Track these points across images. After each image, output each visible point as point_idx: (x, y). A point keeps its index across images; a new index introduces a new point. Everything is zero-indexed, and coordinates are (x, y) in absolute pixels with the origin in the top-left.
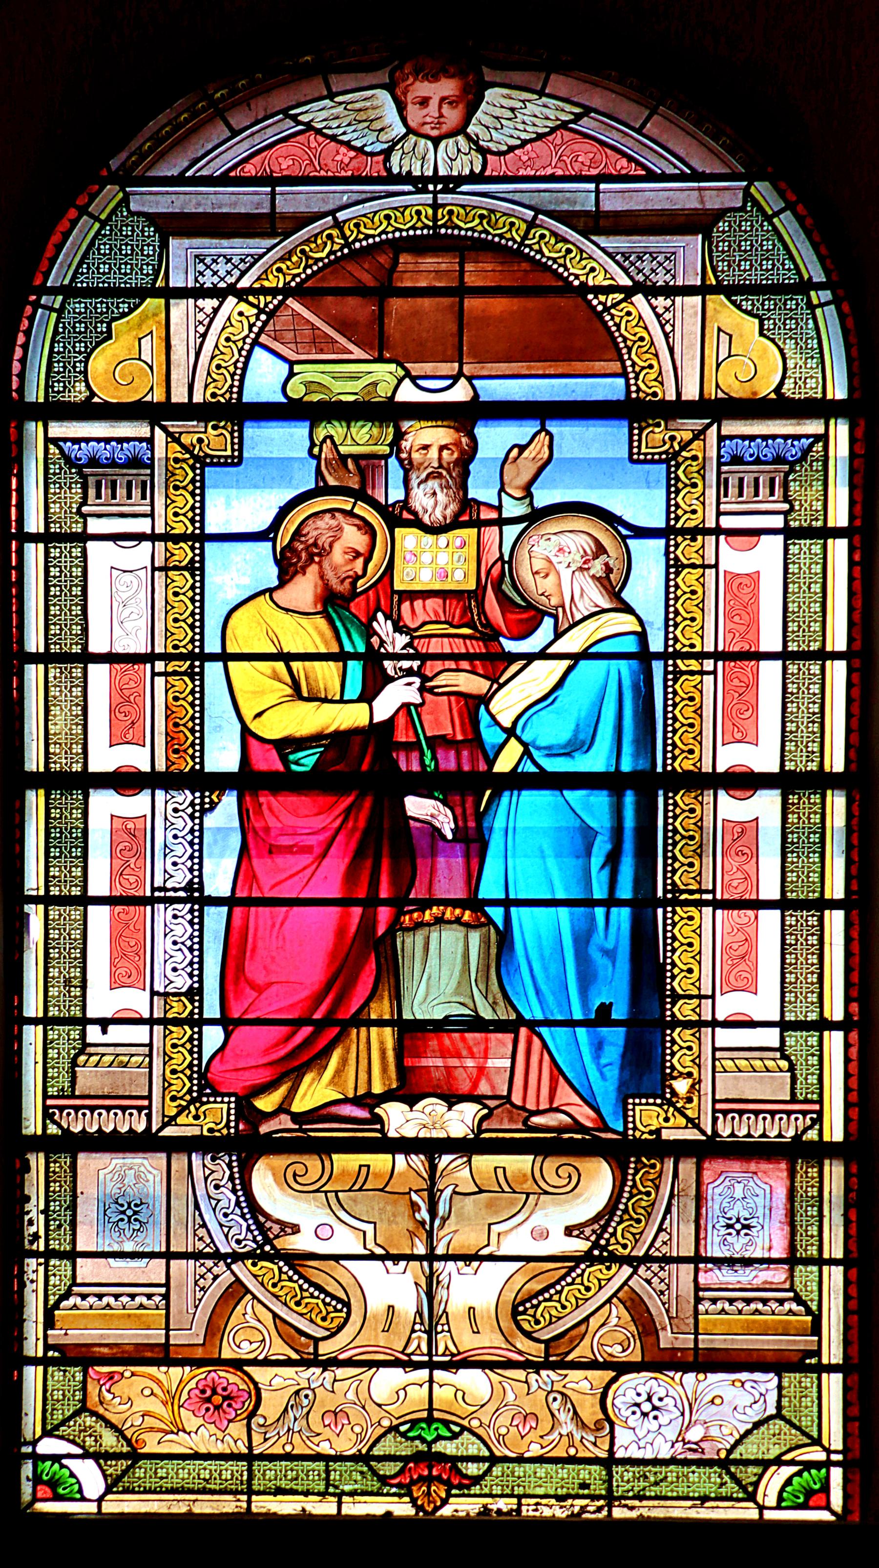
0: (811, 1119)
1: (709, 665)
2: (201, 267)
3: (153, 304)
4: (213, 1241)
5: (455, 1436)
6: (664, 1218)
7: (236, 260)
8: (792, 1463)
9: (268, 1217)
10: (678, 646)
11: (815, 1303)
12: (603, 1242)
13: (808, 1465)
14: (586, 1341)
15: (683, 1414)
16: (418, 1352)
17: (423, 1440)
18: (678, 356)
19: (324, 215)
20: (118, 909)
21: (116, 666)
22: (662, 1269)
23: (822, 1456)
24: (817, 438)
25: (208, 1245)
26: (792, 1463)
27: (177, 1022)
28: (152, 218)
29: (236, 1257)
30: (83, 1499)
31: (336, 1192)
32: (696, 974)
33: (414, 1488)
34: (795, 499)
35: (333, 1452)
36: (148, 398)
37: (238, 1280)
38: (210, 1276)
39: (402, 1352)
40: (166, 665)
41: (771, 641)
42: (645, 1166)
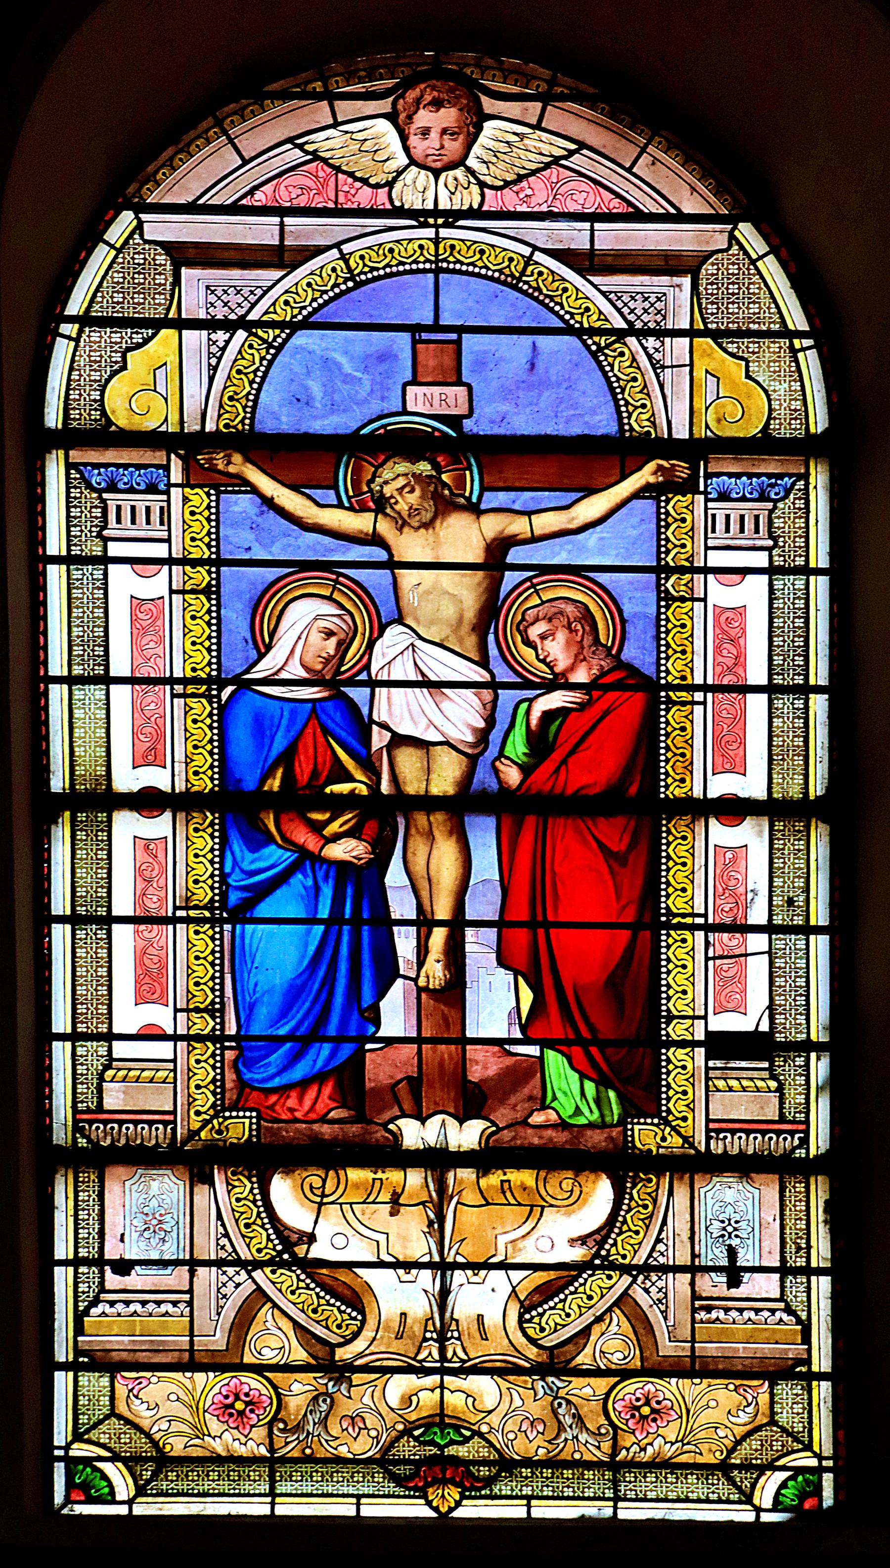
0: (799, 1138)
1: (699, 696)
2: (212, 298)
3: (168, 335)
4: (235, 1251)
5: (467, 1440)
6: (661, 1231)
7: (245, 292)
8: (784, 1468)
9: (287, 1228)
10: (670, 678)
11: (805, 1313)
12: (603, 1253)
13: (799, 1471)
14: (588, 1350)
15: (681, 1417)
16: (430, 1359)
17: (435, 1444)
18: (668, 392)
19: (328, 248)
20: (142, 927)
21: (137, 687)
22: (660, 1278)
23: (814, 1462)
24: (799, 477)
25: (230, 1254)
26: (784, 1468)
27: (199, 1038)
28: (168, 247)
29: (257, 1265)
30: (114, 1502)
31: (351, 1204)
32: (690, 995)
33: (431, 1490)
34: (779, 536)
35: (350, 1456)
36: (163, 428)
37: (259, 1288)
38: (231, 1285)
39: (414, 1359)
40: (185, 689)
41: (757, 674)
42: (642, 1180)
